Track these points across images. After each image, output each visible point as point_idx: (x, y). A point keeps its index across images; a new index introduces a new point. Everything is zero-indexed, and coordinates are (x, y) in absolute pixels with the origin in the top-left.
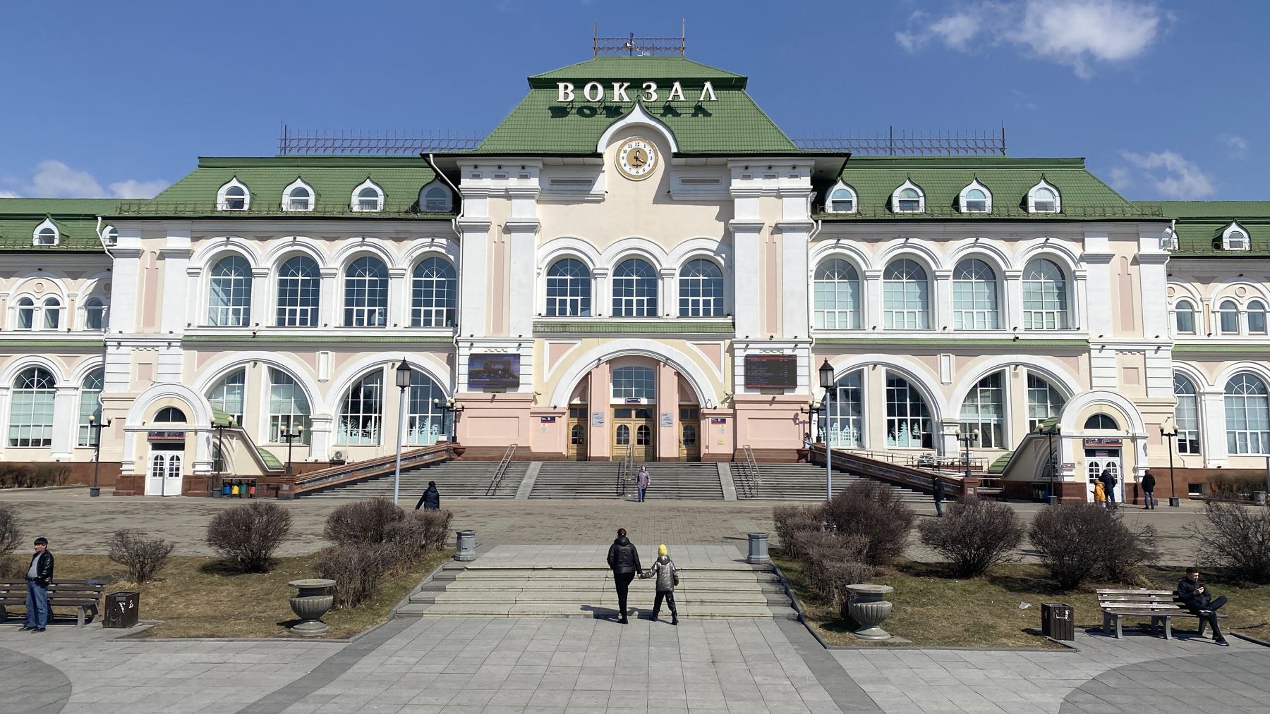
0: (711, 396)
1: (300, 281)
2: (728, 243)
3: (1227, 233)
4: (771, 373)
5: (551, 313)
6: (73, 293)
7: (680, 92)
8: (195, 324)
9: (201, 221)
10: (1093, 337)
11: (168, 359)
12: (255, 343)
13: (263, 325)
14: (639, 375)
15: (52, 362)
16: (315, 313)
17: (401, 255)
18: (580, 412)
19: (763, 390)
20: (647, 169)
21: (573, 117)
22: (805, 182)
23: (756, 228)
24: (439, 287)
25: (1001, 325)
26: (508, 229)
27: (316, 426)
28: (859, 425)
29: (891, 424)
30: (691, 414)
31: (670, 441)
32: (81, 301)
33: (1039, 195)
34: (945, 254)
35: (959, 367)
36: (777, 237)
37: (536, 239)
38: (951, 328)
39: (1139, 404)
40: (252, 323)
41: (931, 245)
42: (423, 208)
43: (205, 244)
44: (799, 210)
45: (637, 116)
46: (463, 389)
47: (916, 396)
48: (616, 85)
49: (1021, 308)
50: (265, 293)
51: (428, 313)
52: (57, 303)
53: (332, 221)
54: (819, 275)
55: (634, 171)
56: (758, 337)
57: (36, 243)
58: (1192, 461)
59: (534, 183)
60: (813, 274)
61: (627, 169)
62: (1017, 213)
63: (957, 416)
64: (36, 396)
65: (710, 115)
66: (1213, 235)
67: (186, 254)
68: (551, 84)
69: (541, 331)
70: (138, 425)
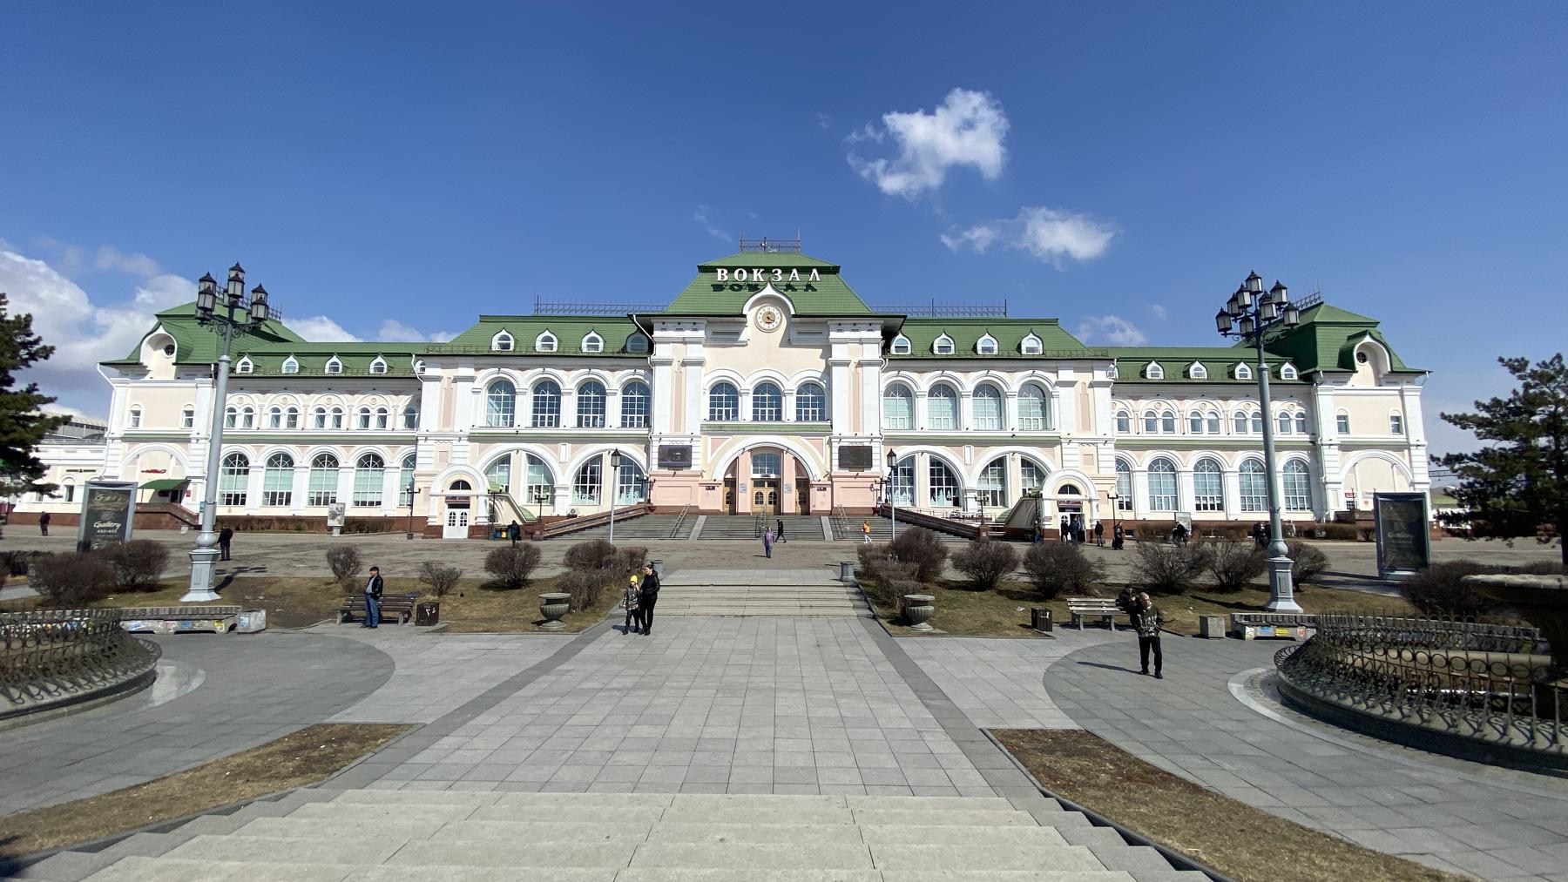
0: (816, 473)
2: (828, 372)
4: (855, 458)
6: (397, 404)
9: (482, 357)
10: (1063, 435)
12: (517, 438)
16: (558, 418)
17: (614, 380)
18: (731, 483)
19: (851, 468)
21: (727, 291)
22: (878, 334)
24: (639, 401)
26: (684, 364)
28: (912, 491)
29: (933, 491)
32: (401, 410)
33: (1029, 342)
34: (968, 381)
43: (484, 372)
44: (874, 352)
47: (948, 472)
54: (887, 394)
58: (1127, 515)
59: (701, 333)
67: (472, 379)
70: (438, 492)
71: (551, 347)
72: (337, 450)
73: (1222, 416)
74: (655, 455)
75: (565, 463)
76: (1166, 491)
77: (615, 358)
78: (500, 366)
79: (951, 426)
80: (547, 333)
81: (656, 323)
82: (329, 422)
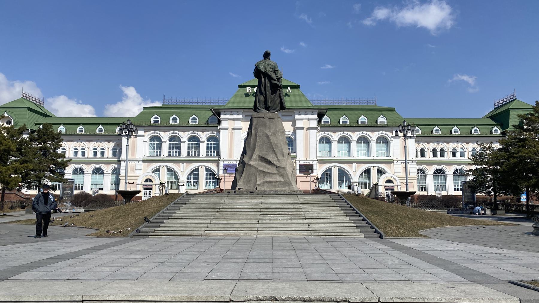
1: (175, 144)
2: (294, 132)
3: (434, 129)
4: (307, 169)
6: (109, 146)
8: (146, 156)
9: (147, 127)
10: (395, 159)
11: (138, 165)
12: (373, 162)
13: (165, 156)
14: (225, 169)
15: (103, 166)
16: (160, 152)
17: (204, 136)
19: (304, 173)
22: (316, 116)
24: (214, 145)
26: (233, 129)
28: (331, 183)
29: (339, 183)
32: (111, 148)
33: (381, 120)
34: (354, 136)
35: (358, 167)
36: (308, 131)
38: (356, 156)
39: (399, 177)
41: (350, 133)
43: (148, 133)
44: (314, 124)
46: (221, 173)
50: (165, 147)
51: (211, 152)
52: (84, 149)
53: (184, 127)
54: (320, 141)
56: (303, 159)
57: (78, 132)
58: (425, 193)
59: (241, 116)
62: (375, 125)
63: (357, 181)
64: (98, 177)
66: (490, 129)
67: (143, 136)
68: (245, 87)
70: (140, 183)
71: (176, 122)
72: (84, 166)
73: (466, 150)
74: (221, 168)
75: (184, 171)
76: (441, 183)
77: (205, 126)
78: (155, 130)
79: (347, 155)
80: (156, 116)
82: (79, 154)
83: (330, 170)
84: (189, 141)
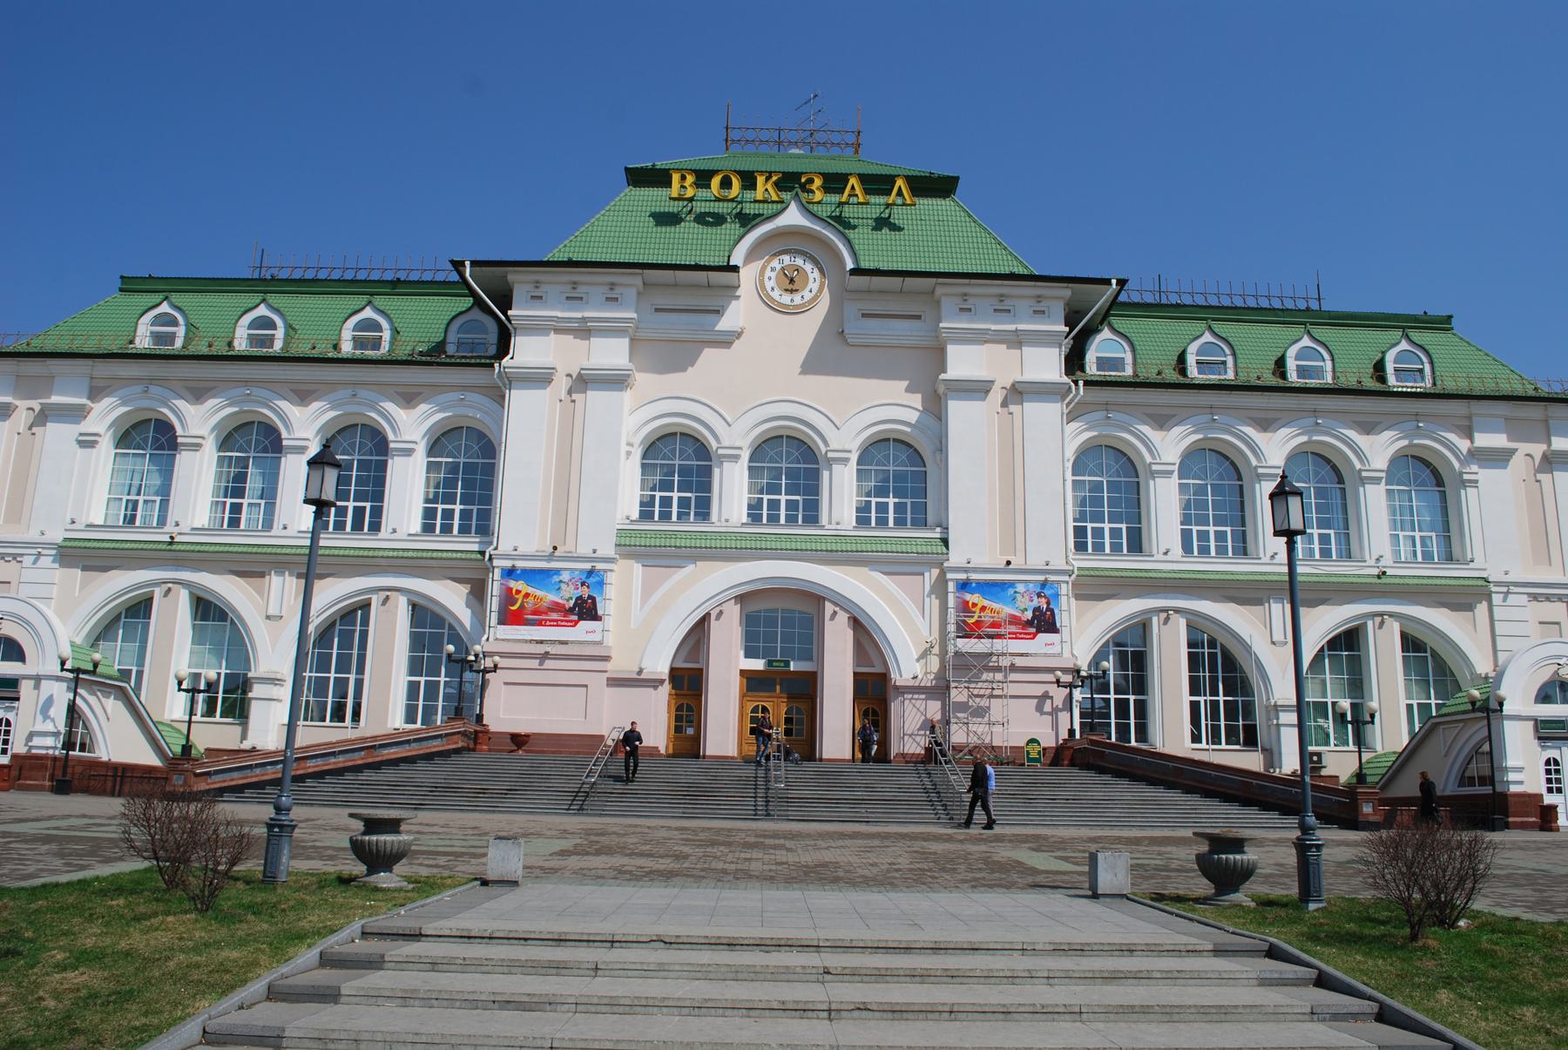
0: (909, 662)
5: (646, 515)
7: (858, 191)
14: (787, 622)
16: (377, 513)
18: (688, 684)
20: (808, 296)
23: (977, 389)
24: (469, 471)
25: (1456, 552)
27: (257, 691)
30: (874, 693)
31: (837, 731)
37: (627, 397)
40: (170, 520)
42: (451, 349)
44: (1047, 365)
45: (793, 216)
47: (1230, 663)
48: (760, 180)
49: (1382, 533)
55: (786, 299)
60: (1069, 465)
61: (776, 294)
65: (900, 229)
69: (631, 547)
81: (521, 284)
83: (1141, 628)
84: (226, 443)
